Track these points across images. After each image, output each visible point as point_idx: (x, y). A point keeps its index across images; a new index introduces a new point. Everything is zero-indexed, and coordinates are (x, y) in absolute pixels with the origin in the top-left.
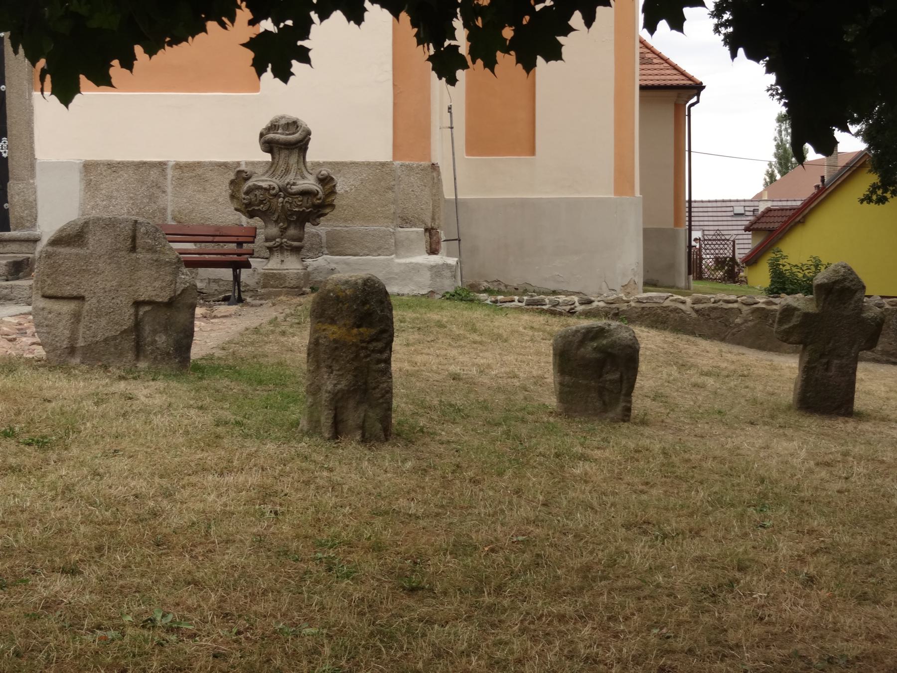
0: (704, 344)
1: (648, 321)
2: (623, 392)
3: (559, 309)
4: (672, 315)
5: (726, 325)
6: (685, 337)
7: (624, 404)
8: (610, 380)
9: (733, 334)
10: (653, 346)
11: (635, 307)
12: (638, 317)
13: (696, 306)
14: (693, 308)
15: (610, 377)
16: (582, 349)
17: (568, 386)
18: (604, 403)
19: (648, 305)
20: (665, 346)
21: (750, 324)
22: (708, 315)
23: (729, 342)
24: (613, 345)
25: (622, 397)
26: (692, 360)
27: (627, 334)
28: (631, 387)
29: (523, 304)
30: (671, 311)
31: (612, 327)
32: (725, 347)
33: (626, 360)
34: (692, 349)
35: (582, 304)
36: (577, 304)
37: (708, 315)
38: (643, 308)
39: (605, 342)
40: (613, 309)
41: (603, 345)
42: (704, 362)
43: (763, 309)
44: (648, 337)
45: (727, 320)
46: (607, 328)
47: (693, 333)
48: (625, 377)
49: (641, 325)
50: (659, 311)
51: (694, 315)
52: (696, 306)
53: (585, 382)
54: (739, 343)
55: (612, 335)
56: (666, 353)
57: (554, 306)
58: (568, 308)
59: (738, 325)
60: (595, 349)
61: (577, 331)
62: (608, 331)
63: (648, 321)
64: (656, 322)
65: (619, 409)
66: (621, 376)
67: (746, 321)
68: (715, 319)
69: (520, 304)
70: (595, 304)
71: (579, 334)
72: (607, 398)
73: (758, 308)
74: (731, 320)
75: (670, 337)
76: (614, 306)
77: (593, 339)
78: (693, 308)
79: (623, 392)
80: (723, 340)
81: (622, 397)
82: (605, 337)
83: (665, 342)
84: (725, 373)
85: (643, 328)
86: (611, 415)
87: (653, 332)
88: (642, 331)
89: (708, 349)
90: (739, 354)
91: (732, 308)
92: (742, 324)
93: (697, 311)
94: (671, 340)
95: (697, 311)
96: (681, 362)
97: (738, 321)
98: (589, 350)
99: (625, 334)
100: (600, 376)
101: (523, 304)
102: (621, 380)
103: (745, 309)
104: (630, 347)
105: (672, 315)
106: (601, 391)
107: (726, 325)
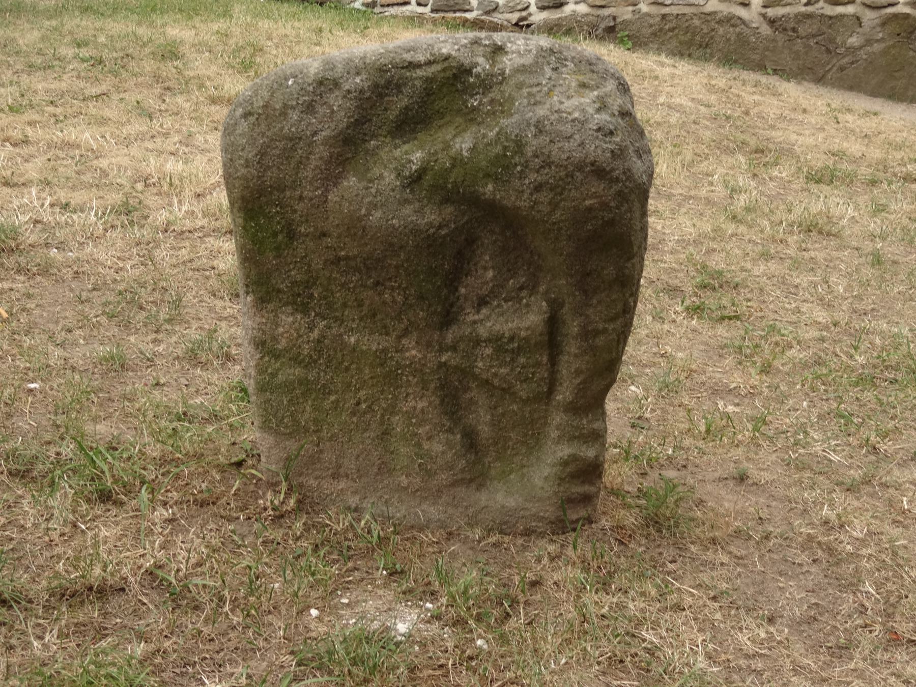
0: (792, 91)
1: (674, 43)
2: (564, 394)
3: (497, 18)
4: (721, 31)
5: (828, 51)
6: (746, 75)
7: (565, 451)
8: (496, 340)
9: (842, 69)
10: (684, 101)
11: (648, 15)
12: (654, 34)
13: (771, 12)
14: (764, 16)
15: (495, 322)
16: (351, 182)
17: (296, 360)
18: (471, 442)
19: (674, 10)
20: (713, 98)
21: (877, 47)
22: (794, 30)
23: (833, 86)
24: (505, 161)
25: (557, 418)
26: (778, 135)
27: (587, 99)
28: (605, 369)
29: (427, 10)
30: (720, 22)
31: (508, 63)
32: (837, 98)
33: (579, 236)
34: (771, 107)
35: (542, 8)
36: (533, 8)
37: (794, 30)
38: (664, 16)
39: (464, 144)
40: (604, 19)
41: (457, 161)
42: (810, 141)
43: (907, 16)
44: (673, 76)
45: (832, 40)
46: (482, 65)
47: (760, 67)
48: (573, 327)
49: (659, 51)
50: (696, 22)
51: (766, 30)
52: (771, 12)
53: (373, 343)
54: (853, 86)
55: (502, 107)
56: (715, 118)
57: (488, 13)
58: (514, 17)
59: (852, 50)
60: (416, 179)
61: (326, 84)
62: (486, 84)
63: (674, 43)
64: (690, 44)
65: (537, 478)
66: (553, 323)
67: (869, 42)
68: (807, 37)
69: (420, 10)
70: (568, 9)
71: (335, 100)
72: (482, 420)
73: (895, 16)
74: (839, 40)
75: (720, 77)
76: (606, 12)
77: (409, 125)
78: (764, 16)
79: (564, 394)
80: (820, 80)
81: (557, 418)
82: (472, 116)
83: (711, 89)
84: (864, 171)
85: (663, 58)
86: (501, 497)
87: (684, 67)
88: (662, 64)
89: (805, 104)
90: (867, 114)
91: (842, 16)
92: (861, 47)
93: (772, 22)
94: (721, 83)
95: (772, 22)
96: (753, 142)
97: (854, 41)
98: (381, 189)
99: (575, 103)
100: (448, 318)
101: (427, 10)
102: (552, 336)
103: (869, 17)
104: (600, 172)
105: (721, 31)
106: (452, 392)
107: (828, 51)
